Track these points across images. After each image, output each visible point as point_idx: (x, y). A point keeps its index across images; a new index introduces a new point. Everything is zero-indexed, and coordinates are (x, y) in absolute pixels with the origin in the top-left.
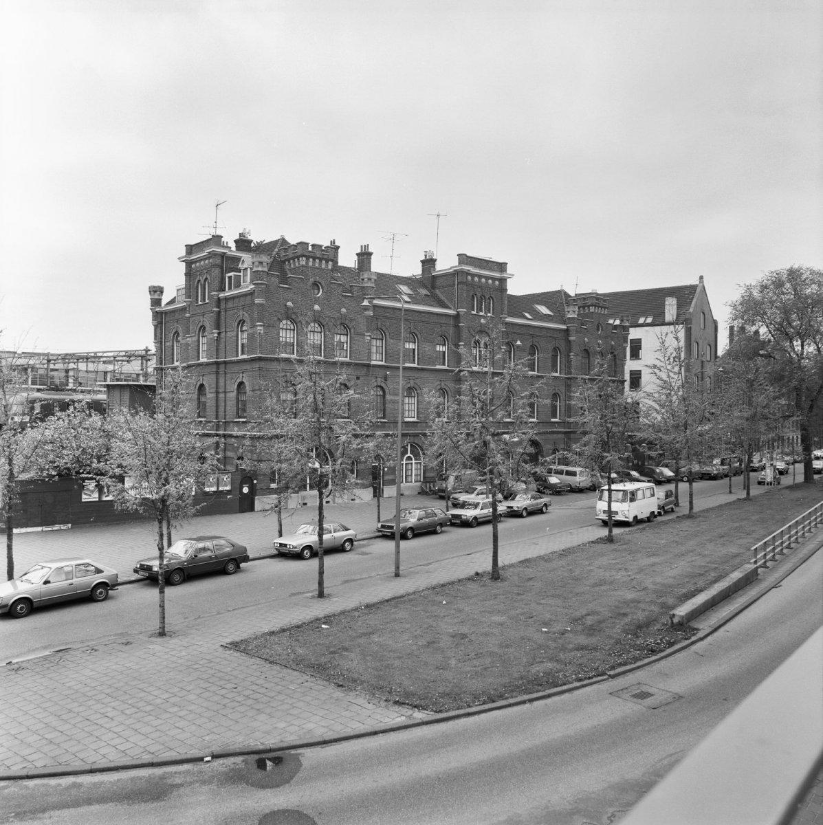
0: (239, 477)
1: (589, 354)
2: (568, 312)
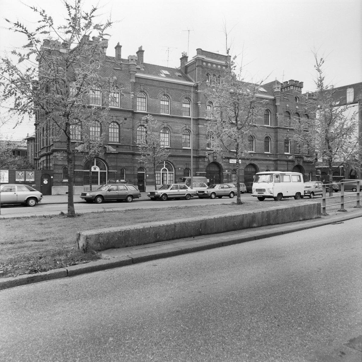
0: (40, 174)
1: (289, 114)
2: (275, 88)
